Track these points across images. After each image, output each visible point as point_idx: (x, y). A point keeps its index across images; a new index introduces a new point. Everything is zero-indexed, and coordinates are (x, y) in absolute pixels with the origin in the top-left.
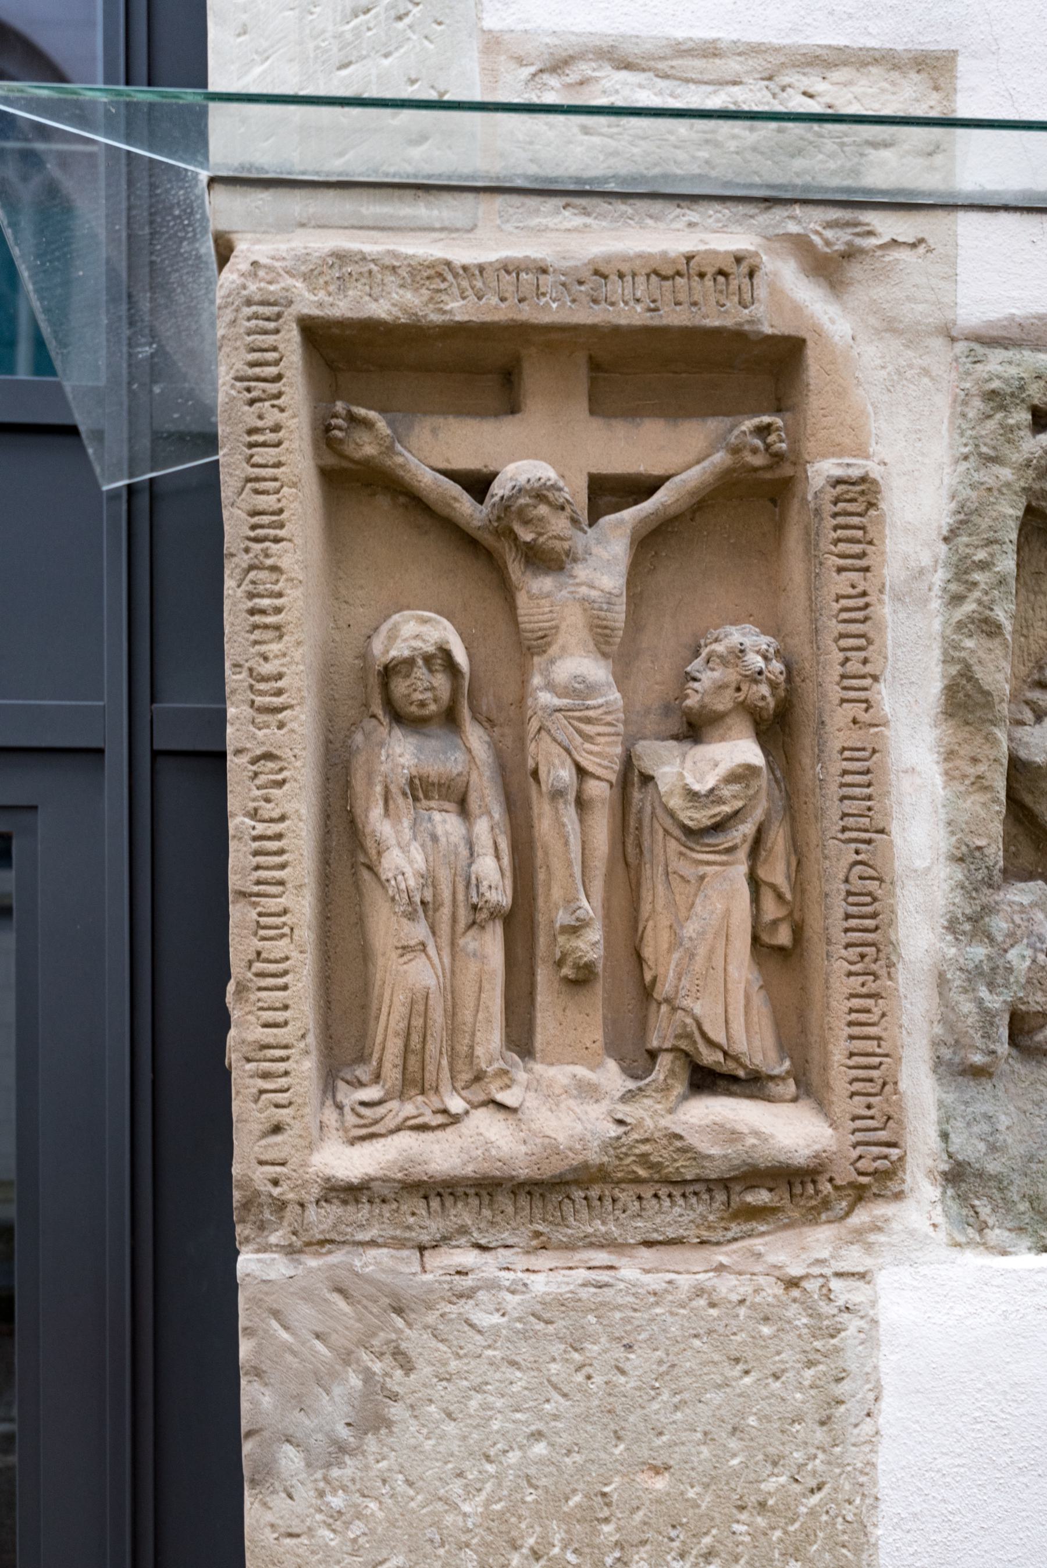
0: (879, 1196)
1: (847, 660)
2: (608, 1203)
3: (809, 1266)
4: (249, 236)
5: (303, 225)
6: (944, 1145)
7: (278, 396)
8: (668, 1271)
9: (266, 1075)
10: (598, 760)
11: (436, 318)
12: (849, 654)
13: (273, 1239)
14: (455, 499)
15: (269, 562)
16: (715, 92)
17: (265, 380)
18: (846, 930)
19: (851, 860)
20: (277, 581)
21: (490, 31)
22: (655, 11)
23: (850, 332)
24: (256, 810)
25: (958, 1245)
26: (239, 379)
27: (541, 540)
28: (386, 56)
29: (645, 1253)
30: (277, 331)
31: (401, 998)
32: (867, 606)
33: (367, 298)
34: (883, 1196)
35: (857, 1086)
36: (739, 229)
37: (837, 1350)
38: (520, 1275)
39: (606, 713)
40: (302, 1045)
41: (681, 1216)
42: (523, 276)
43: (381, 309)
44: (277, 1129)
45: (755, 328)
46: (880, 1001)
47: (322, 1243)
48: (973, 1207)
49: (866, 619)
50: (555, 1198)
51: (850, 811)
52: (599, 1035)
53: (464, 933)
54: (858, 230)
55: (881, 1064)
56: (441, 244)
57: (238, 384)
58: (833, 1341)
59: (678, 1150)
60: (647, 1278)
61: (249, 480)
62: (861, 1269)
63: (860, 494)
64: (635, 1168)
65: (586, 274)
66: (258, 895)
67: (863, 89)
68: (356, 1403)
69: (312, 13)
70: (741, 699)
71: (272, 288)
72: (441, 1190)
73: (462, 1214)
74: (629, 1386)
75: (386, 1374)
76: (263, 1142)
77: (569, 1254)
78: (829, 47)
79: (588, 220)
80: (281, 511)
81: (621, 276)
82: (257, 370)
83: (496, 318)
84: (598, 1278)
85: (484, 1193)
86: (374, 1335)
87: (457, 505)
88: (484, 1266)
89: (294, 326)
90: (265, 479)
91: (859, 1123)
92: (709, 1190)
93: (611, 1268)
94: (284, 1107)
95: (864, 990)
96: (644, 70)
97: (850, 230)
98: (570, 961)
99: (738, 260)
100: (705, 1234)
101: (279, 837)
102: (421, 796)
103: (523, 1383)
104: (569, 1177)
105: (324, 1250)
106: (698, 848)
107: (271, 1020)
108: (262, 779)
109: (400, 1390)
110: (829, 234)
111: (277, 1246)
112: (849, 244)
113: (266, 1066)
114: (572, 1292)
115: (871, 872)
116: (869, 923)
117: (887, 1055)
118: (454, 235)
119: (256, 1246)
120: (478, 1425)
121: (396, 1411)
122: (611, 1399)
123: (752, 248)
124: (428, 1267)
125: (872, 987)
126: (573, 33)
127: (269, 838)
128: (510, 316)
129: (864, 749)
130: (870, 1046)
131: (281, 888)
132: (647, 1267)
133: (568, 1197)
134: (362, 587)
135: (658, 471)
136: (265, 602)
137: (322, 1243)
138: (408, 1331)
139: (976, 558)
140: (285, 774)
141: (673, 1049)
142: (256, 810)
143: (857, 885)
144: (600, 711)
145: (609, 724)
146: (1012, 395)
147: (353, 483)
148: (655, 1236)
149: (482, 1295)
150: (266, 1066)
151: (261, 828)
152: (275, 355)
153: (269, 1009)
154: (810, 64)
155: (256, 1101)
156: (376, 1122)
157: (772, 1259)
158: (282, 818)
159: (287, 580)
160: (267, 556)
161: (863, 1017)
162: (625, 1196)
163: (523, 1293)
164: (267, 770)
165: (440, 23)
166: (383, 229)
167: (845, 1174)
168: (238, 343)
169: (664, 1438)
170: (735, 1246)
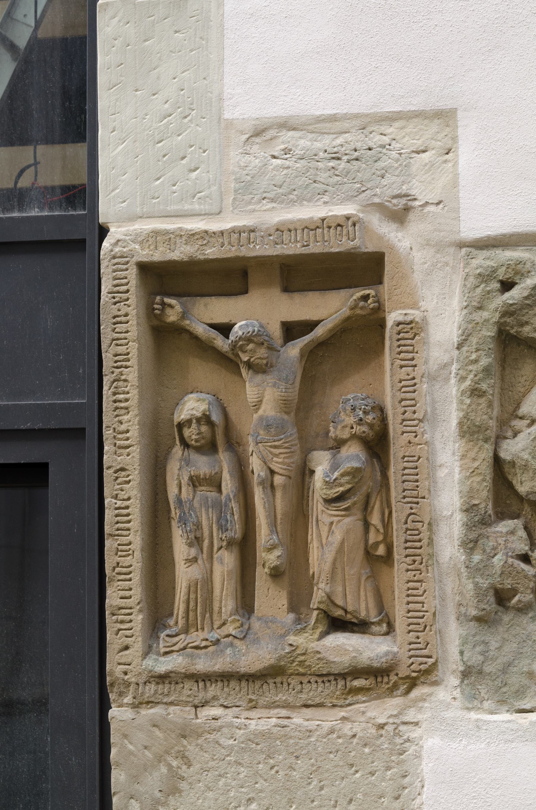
0: (424, 683)
1: (405, 412)
2: (285, 685)
3: (389, 717)
4: (115, 224)
5: (141, 217)
6: (461, 657)
7: (127, 299)
8: (318, 720)
9: (122, 622)
10: (280, 466)
11: (202, 257)
12: (406, 409)
13: (125, 701)
14: (214, 339)
15: (123, 377)
16: (336, 138)
17: (121, 293)
18: (406, 548)
19: (408, 513)
20: (127, 386)
21: (227, 119)
22: (306, 103)
23: (409, 246)
24: (117, 495)
25: (468, 709)
26: (109, 293)
27: (252, 360)
28: (179, 135)
29: (305, 710)
30: (127, 270)
31: (184, 585)
32: (415, 384)
33: (168, 251)
34: (426, 683)
35: (412, 627)
36: (349, 203)
37: (403, 761)
38: (243, 720)
39: (284, 443)
40: (138, 607)
41: (322, 692)
42: (242, 234)
43: (176, 255)
44: (127, 648)
45: (357, 251)
46: (424, 584)
47: (148, 703)
48: (478, 689)
49: (414, 392)
50: (258, 683)
51: (408, 488)
52: (285, 602)
53: (217, 552)
54: (409, 198)
55: (424, 616)
56: (204, 222)
57: (110, 295)
58: (401, 757)
59: (319, 659)
60: (306, 723)
61: (114, 340)
62: (415, 720)
63: (412, 329)
64: (298, 668)
65: (272, 231)
66: (118, 535)
67: (410, 130)
68: (164, 781)
69: (145, 119)
70: (353, 433)
71: (125, 250)
72: (205, 679)
73: (213, 690)
74: (297, 776)
75: (178, 767)
76: (120, 654)
77: (267, 711)
78: (393, 112)
79: (274, 205)
80: (128, 354)
81: (290, 231)
82: (118, 288)
83: (229, 256)
84: (282, 723)
85: (225, 680)
86: (173, 748)
87: (215, 341)
88: (228, 716)
89: (135, 267)
90: (121, 339)
91: (412, 646)
92: (336, 680)
93: (289, 718)
94: (130, 637)
95: (416, 578)
96: (302, 130)
97: (405, 199)
98: (267, 565)
99: (348, 218)
100: (335, 701)
101: (127, 507)
102: (197, 484)
103: (245, 774)
104: (265, 672)
105: (149, 707)
106: (330, 508)
107: (124, 596)
108: (119, 481)
109: (185, 775)
110: (395, 201)
111: (127, 704)
112: (406, 204)
113: (121, 617)
114: (268, 729)
115: (418, 518)
116: (418, 544)
117: (427, 612)
118: (210, 217)
119: (118, 704)
120: (223, 794)
121: (183, 785)
122: (288, 783)
123: (354, 212)
124: (199, 716)
125: (421, 577)
126: (266, 118)
127: (123, 508)
128: (236, 254)
129: (415, 456)
130: (418, 606)
131: (128, 532)
132: (307, 718)
133: (266, 682)
134: (175, 379)
135: (315, 318)
136: (121, 396)
137: (148, 703)
138: (189, 747)
139: (471, 358)
140: (130, 477)
141: (318, 609)
142: (117, 495)
143: (410, 525)
144: (281, 442)
145: (286, 448)
146: (488, 275)
147: (165, 336)
148: (310, 702)
149: (225, 730)
150: (121, 617)
151: (119, 503)
152: (126, 281)
153: (123, 590)
154: (383, 120)
155: (117, 634)
156: (175, 645)
157: (369, 714)
158: (129, 499)
159: (131, 386)
160: (122, 375)
161: (415, 592)
162: (294, 681)
163: (245, 729)
164: (122, 476)
165: (204, 118)
166: (177, 216)
167: (403, 672)
168: (110, 276)
169: (315, 803)
170: (349, 708)
